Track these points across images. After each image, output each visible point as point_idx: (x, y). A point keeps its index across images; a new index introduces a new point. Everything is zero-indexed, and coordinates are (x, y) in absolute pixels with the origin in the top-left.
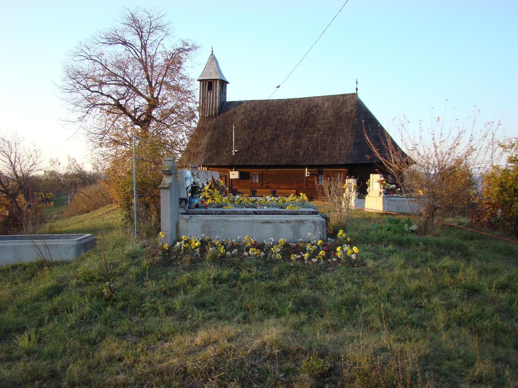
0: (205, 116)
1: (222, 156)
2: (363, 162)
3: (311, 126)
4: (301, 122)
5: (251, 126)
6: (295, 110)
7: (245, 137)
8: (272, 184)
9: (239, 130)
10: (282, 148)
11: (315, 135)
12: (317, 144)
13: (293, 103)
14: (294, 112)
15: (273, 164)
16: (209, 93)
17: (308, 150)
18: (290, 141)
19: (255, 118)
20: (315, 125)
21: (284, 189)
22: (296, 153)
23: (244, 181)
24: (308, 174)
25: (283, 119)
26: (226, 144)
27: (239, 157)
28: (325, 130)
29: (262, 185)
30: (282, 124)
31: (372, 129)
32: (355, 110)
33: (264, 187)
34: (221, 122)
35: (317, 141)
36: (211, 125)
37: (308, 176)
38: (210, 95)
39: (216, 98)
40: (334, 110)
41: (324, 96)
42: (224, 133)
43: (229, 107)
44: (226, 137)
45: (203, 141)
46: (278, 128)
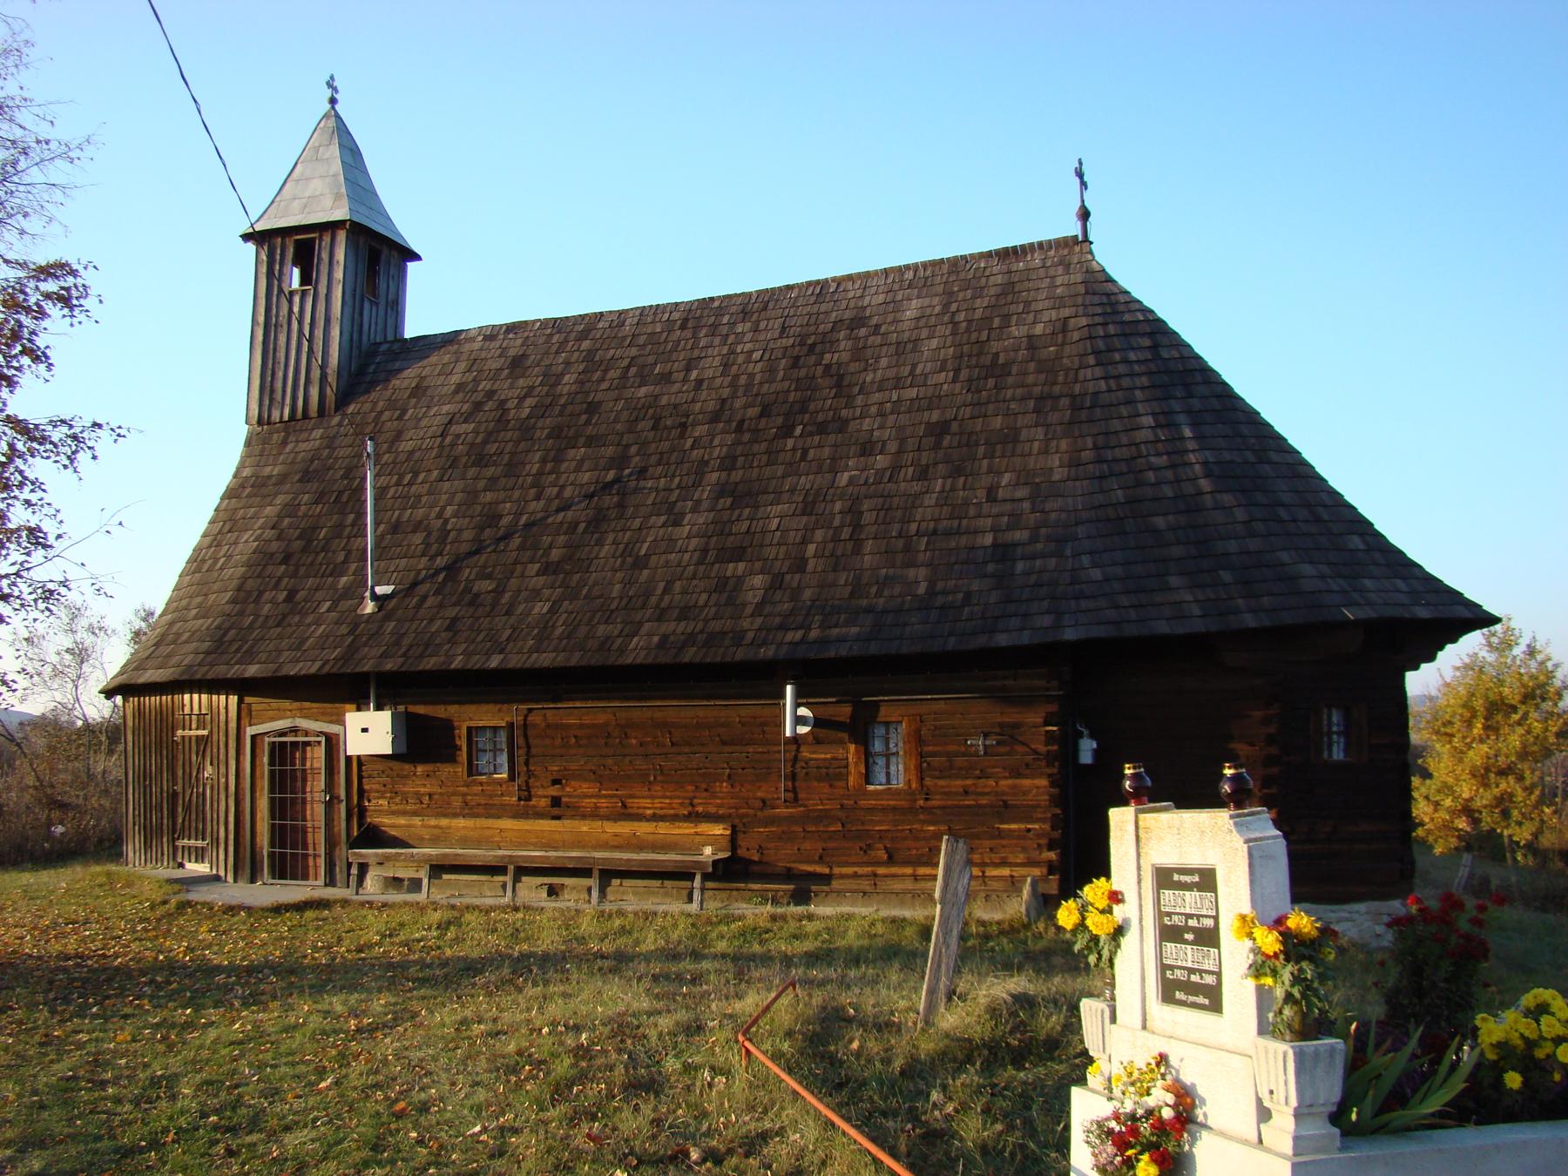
1: (309, 619)
2: (1162, 628)
3: (822, 429)
4: (765, 412)
6: (732, 352)
8: (586, 788)
9: (422, 476)
10: (640, 563)
11: (843, 479)
13: (725, 320)
14: (726, 366)
15: (575, 660)
17: (800, 565)
18: (694, 521)
19: (518, 407)
21: (655, 818)
22: (722, 584)
23: (429, 767)
24: (799, 720)
25: (664, 400)
26: (341, 557)
28: (902, 441)
30: (654, 428)
31: (1194, 425)
32: (1084, 321)
33: (544, 802)
35: (853, 511)
39: (328, 320)
41: (901, 270)
42: (344, 498)
43: (397, 365)
44: (352, 516)
46: (633, 449)
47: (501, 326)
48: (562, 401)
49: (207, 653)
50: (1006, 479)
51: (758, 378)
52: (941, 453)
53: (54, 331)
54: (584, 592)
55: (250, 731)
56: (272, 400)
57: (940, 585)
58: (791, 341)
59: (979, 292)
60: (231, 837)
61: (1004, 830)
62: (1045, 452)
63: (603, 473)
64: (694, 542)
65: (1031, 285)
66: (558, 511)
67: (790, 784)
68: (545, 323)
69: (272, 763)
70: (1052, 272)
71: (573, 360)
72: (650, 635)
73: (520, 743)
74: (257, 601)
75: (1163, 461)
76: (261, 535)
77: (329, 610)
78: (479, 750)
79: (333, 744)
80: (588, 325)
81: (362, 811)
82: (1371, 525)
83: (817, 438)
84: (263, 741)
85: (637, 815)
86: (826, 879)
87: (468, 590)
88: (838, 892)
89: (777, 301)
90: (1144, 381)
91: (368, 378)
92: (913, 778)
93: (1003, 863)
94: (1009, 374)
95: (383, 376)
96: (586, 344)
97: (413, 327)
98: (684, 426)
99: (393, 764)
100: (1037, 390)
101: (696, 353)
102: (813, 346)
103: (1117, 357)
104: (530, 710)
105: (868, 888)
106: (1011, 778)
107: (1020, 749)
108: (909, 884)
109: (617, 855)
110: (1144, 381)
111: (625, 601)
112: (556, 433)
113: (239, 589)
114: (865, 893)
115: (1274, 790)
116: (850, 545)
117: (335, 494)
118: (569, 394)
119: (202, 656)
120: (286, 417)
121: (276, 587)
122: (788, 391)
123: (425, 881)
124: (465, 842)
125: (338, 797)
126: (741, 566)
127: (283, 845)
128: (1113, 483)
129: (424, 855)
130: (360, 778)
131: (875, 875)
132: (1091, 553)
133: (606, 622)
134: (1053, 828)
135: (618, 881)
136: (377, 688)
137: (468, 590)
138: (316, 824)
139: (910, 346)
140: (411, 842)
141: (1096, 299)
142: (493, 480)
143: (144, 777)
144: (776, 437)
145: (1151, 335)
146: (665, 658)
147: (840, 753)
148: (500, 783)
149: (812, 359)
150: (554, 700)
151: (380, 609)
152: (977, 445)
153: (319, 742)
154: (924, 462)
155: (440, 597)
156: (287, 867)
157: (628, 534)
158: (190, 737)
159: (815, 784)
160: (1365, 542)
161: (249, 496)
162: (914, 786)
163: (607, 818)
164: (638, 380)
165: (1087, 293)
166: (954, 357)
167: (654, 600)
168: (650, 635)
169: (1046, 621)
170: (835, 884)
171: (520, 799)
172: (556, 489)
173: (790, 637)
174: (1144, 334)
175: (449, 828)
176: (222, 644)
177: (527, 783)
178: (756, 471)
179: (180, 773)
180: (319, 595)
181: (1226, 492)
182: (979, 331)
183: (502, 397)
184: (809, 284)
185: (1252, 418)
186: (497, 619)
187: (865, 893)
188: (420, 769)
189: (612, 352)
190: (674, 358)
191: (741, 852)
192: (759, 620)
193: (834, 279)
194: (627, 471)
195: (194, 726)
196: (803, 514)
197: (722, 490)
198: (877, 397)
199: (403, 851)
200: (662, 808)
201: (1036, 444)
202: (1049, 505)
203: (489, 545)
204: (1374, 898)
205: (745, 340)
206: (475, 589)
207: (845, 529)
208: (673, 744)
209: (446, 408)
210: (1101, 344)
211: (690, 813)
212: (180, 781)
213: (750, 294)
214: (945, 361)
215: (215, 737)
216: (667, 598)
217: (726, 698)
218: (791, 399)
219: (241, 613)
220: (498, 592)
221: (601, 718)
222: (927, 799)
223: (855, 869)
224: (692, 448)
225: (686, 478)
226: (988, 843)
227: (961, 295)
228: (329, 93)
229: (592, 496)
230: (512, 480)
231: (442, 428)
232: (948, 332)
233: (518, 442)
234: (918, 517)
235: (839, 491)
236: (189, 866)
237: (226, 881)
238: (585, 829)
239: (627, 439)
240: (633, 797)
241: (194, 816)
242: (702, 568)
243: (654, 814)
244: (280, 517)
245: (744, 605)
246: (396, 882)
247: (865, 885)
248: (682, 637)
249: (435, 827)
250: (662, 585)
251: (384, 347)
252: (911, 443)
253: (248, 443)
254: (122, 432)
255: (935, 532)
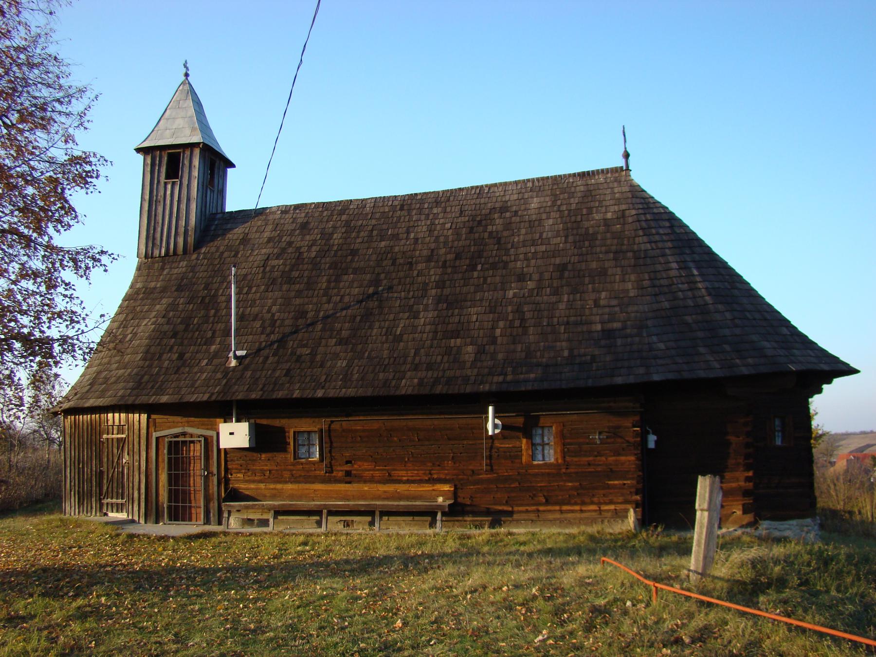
0: (156, 253)
1: (196, 370)
2: (702, 374)
3: (494, 266)
4: (458, 257)
5: (295, 274)
6: (432, 224)
7: (274, 309)
8: (366, 465)
9: (254, 289)
10: (398, 339)
11: (510, 294)
12: (523, 320)
13: (426, 206)
14: (430, 231)
15: (369, 392)
16: (169, 187)
17: (494, 341)
18: (426, 317)
19: (309, 251)
20: (506, 263)
21: (408, 482)
22: (448, 351)
23: (269, 455)
24: (495, 426)
25: (397, 249)
26: (210, 334)
27: (248, 374)
28: (541, 274)
29: (330, 469)
30: (393, 264)
31: (698, 268)
32: (633, 212)
33: (340, 474)
34: (202, 268)
35: (518, 310)
36: (169, 280)
37: (497, 431)
38: (170, 191)
39: (188, 200)
40: (561, 217)
41: (525, 182)
42: (207, 300)
43: (229, 226)
44: (213, 312)
45: (142, 328)
46: (383, 276)
47: (291, 206)
48: (335, 248)
49: (133, 389)
50: (603, 295)
51: (450, 238)
52: (564, 281)
53: (76, 197)
54: (366, 355)
55: (155, 435)
56: (154, 244)
57: (576, 352)
58: (467, 218)
59: (572, 195)
60: (143, 496)
61: (611, 484)
62: (623, 281)
63: (366, 289)
64: (428, 328)
65: (601, 192)
66: (342, 309)
67: (488, 461)
68: (318, 205)
69: (169, 453)
70: (611, 185)
71: (338, 225)
72: (412, 378)
73: (328, 440)
74: (160, 358)
75: (685, 286)
76: (156, 322)
77: (207, 365)
78: (299, 445)
79: (210, 443)
80: (343, 207)
81: (227, 481)
82: (790, 322)
83: (491, 272)
84: (164, 441)
85: (397, 480)
86: (510, 514)
87: (293, 353)
88: (517, 521)
89: (455, 196)
90: (669, 244)
91: (212, 233)
92: (559, 457)
93: (611, 502)
94: (597, 239)
95: (220, 232)
96: (344, 217)
97: (233, 204)
98: (411, 264)
99: (246, 453)
100: (614, 248)
101: (412, 224)
102: (480, 221)
103: (654, 231)
104: (332, 422)
105: (534, 518)
106: (614, 456)
107: (619, 440)
108: (558, 516)
109: (386, 503)
110: (669, 244)
111: (392, 360)
112: (334, 266)
113: (147, 352)
114: (532, 521)
115: (751, 461)
116: (520, 330)
117: (200, 299)
118: (339, 245)
119: (129, 391)
120: (163, 254)
121: (170, 350)
122: (470, 246)
123: (271, 520)
124: (292, 497)
125: (212, 473)
126: (459, 340)
127: (177, 501)
128: (662, 298)
129: (270, 505)
130: (226, 461)
131: (538, 511)
132: (657, 335)
133: (383, 371)
134: (638, 483)
135: (387, 518)
136: (237, 410)
137: (293, 353)
138: (197, 488)
139: (537, 223)
140: (258, 498)
141: (638, 201)
142: (299, 293)
143: (79, 462)
144: (466, 270)
145: (669, 220)
146: (426, 391)
147: (517, 444)
148: (314, 463)
149: (481, 229)
150: (347, 416)
151: (240, 364)
152: (584, 277)
153: (200, 441)
154: (555, 285)
155: (277, 358)
156: (178, 514)
157: (387, 323)
158: (113, 439)
159: (503, 461)
160: (790, 331)
161: (142, 299)
162: (560, 461)
163: (379, 482)
164: (379, 238)
165: (633, 197)
166: (563, 230)
167: (409, 359)
168: (412, 378)
169: (642, 370)
170: (515, 516)
171: (326, 472)
172: (339, 298)
173: (496, 379)
174: (666, 220)
175: (283, 489)
176: (141, 383)
177: (330, 463)
178: (458, 289)
179: (105, 460)
180: (199, 356)
181: (720, 303)
182: (576, 216)
183: (298, 245)
184: (472, 188)
185: (724, 265)
186: (316, 369)
187: (532, 521)
188: (263, 456)
189: (361, 222)
190: (399, 226)
191: (460, 500)
192: (475, 371)
193: (486, 186)
194: (380, 288)
195: (115, 432)
196: (490, 313)
197: (439, 300)
198: (522, 250)
199: (256, 503)
200: (412, 476)
201: (617, 277)
202: (630, 309)
203: (302, 329)
204: (799, 518)
205: (439, 217)
206: (298, 353)
207: (516, 321)
208: (419, 440)
209: (263, 251)
210: (644, 224)
211: (429, 479)
212: (105, 465)
213: (438, 192)
214: (558, 231)
215: (131, 439)
216: (417, 359)
217: (451, 414)
218: (472, 250)
219: (150, 366)
220: (313, 354)
221: (375, 426)
222: (567, 468)
223: (527, 508)
224: (418, 276)
225: (416, 292)
226: (602, 492)
227: (562, 197)
228: (184, 70)
229: (361, 301)
230: (311, 292)
231: (262, 263)
232: (558, 216)
233: (312, 270)
234: (557, 315)
235: (508, 300)
236: (110, 514)
237: (139, 523)
238: (366, 489)
239: (377, 270)
240: (396, 470)
241: (115, 485)
242: (435, 342)
243: (408, 480)
244: (167, 311)
245: (464, 362)
246: (249, 522)
247: (532, 516)
248: (432, 380)
249: (272, 489)
250: (413, 351)
251: (219, 216)
252: (547, 276)
253: (139, 269)
254: (116, 257)
255: (568, 323)
